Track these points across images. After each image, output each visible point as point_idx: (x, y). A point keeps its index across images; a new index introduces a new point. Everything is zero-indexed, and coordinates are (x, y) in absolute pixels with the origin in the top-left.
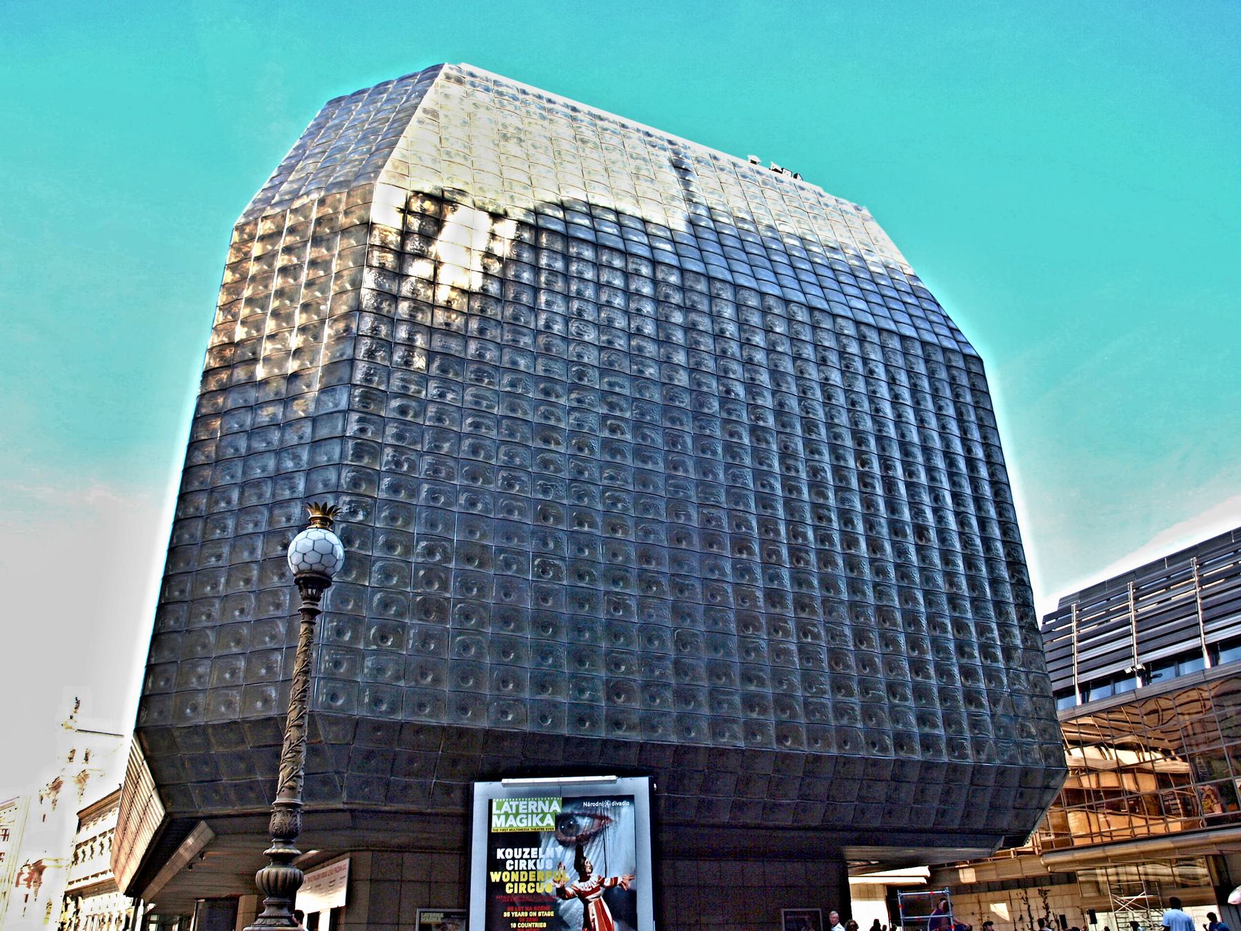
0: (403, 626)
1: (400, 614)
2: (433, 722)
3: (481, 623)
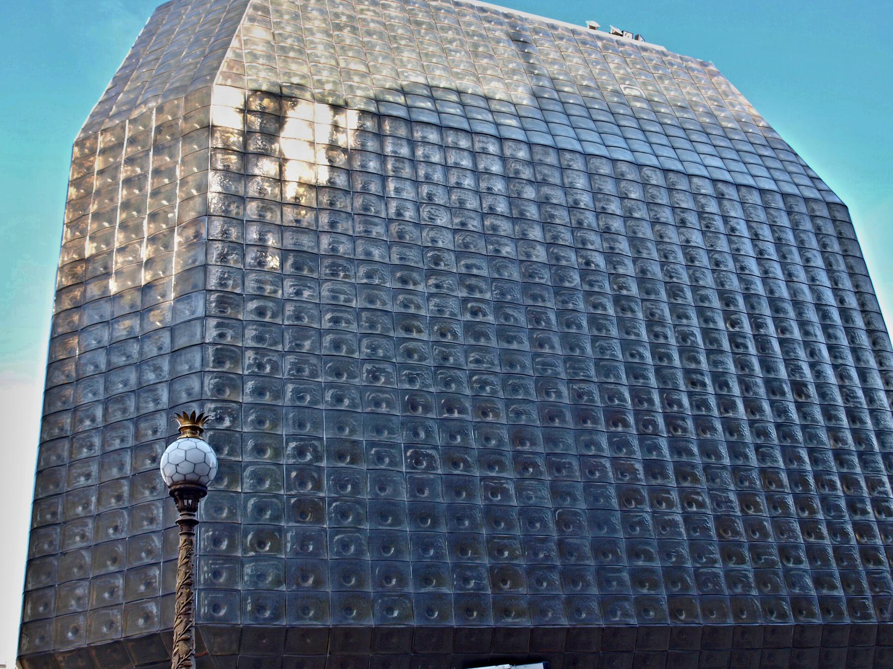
3: (358, 520)
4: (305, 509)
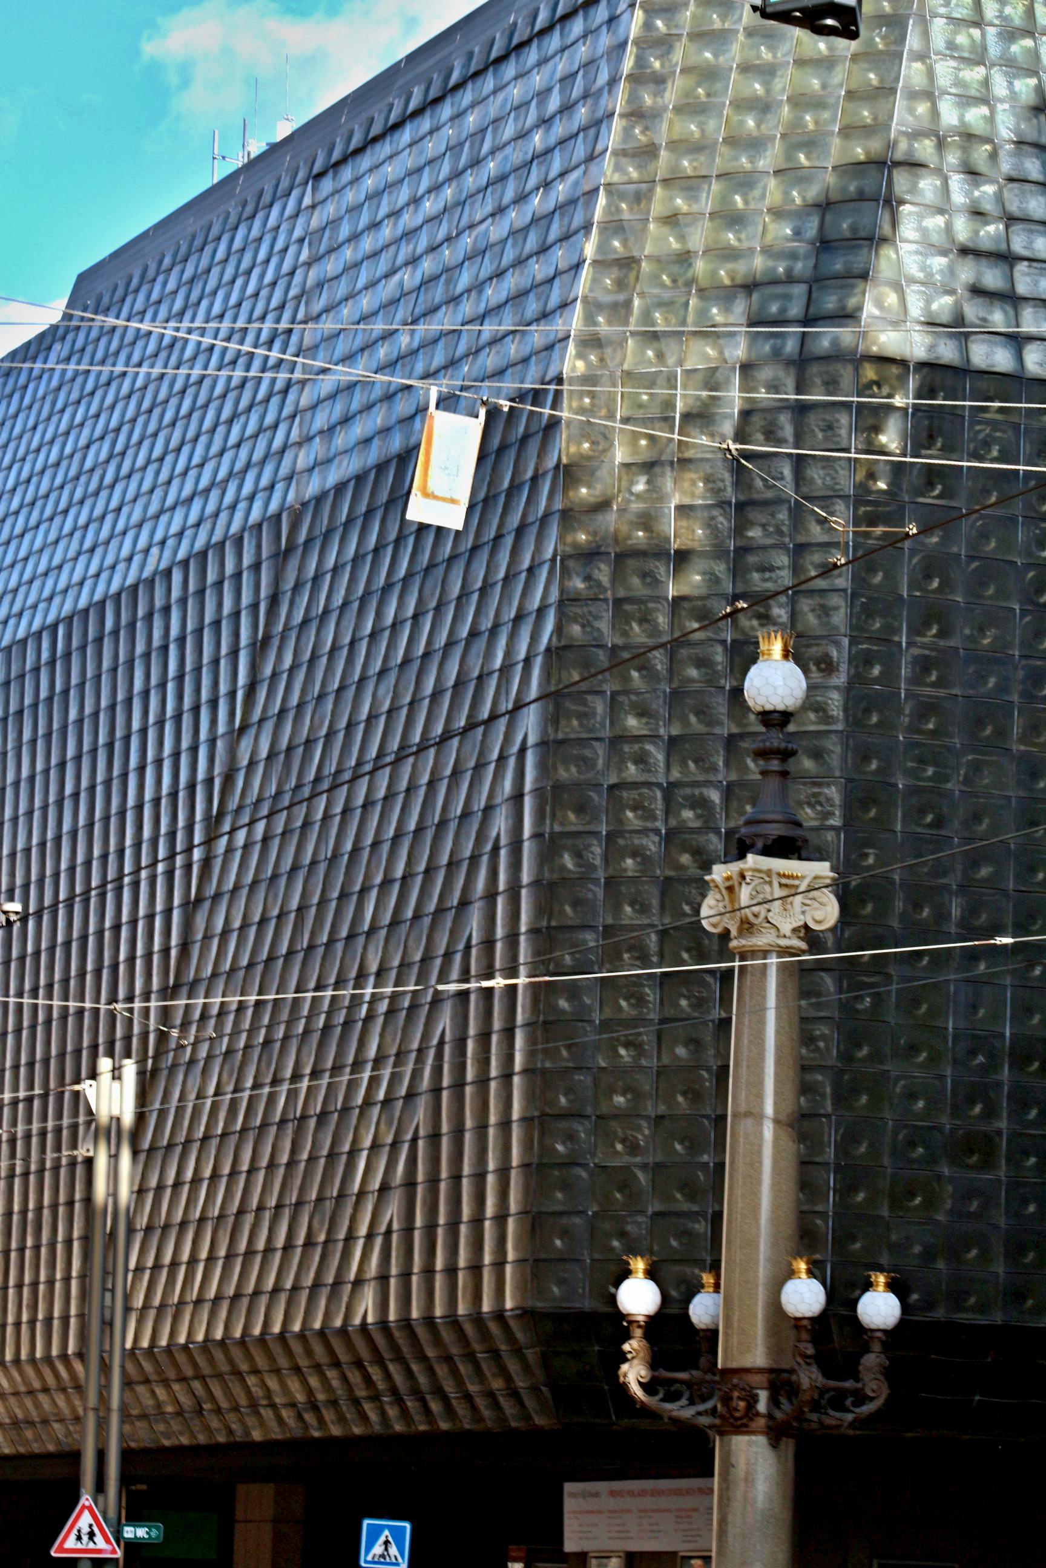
0: (939, 1178)
1: (931, 1159)
2: (982, 1320)
4: (977, 1147)
